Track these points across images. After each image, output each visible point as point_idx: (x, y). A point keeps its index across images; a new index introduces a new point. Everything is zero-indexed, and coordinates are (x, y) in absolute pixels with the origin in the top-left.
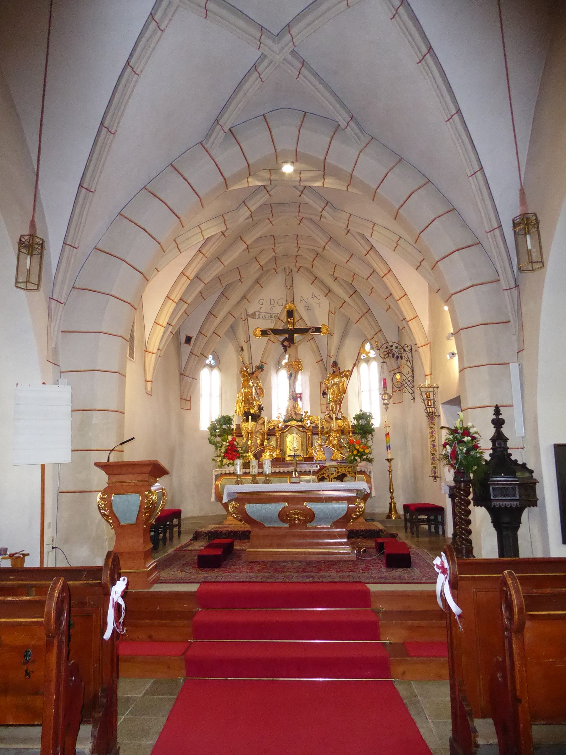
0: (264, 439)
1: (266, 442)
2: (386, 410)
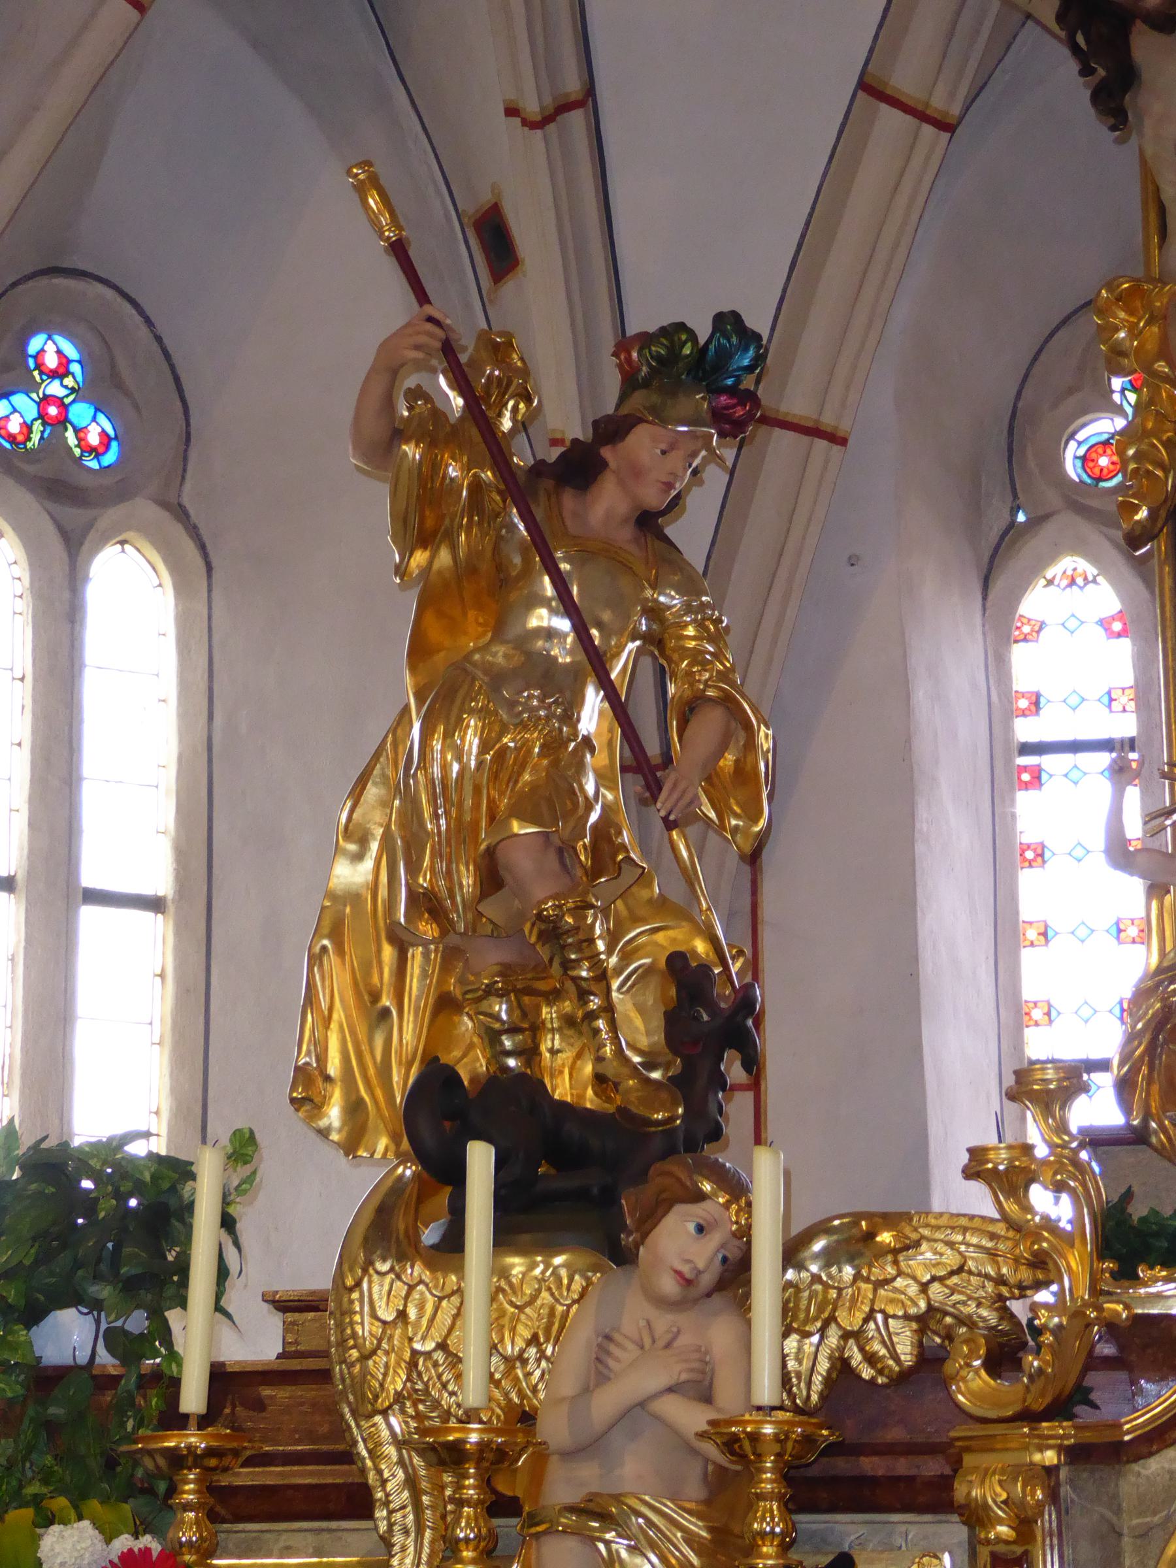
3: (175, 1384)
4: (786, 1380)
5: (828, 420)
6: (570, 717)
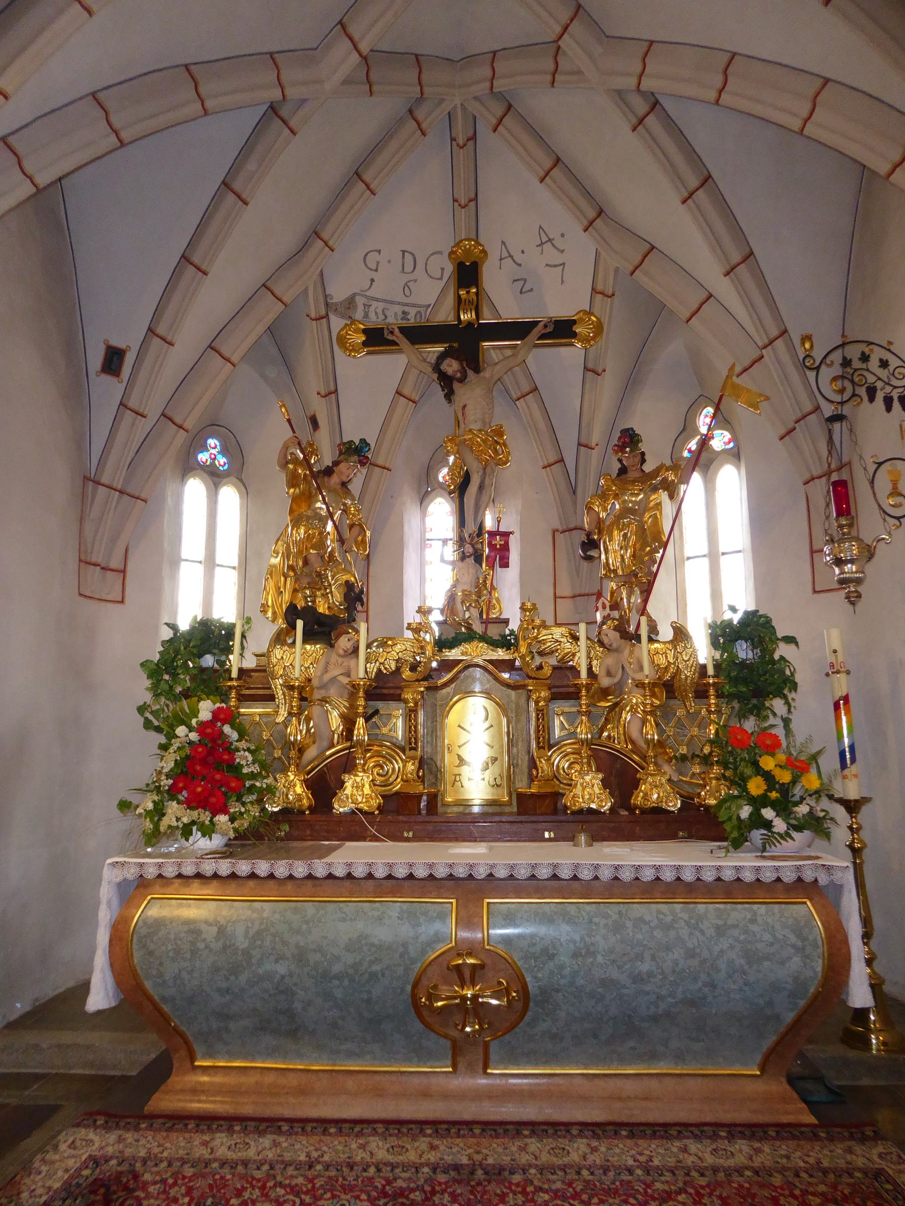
0: (357, 715)
1: (360, 729)
2: (853, 603)
3: (231, 671)
4: (366, 672)
5: (387, 466)
6: (324, 527)
